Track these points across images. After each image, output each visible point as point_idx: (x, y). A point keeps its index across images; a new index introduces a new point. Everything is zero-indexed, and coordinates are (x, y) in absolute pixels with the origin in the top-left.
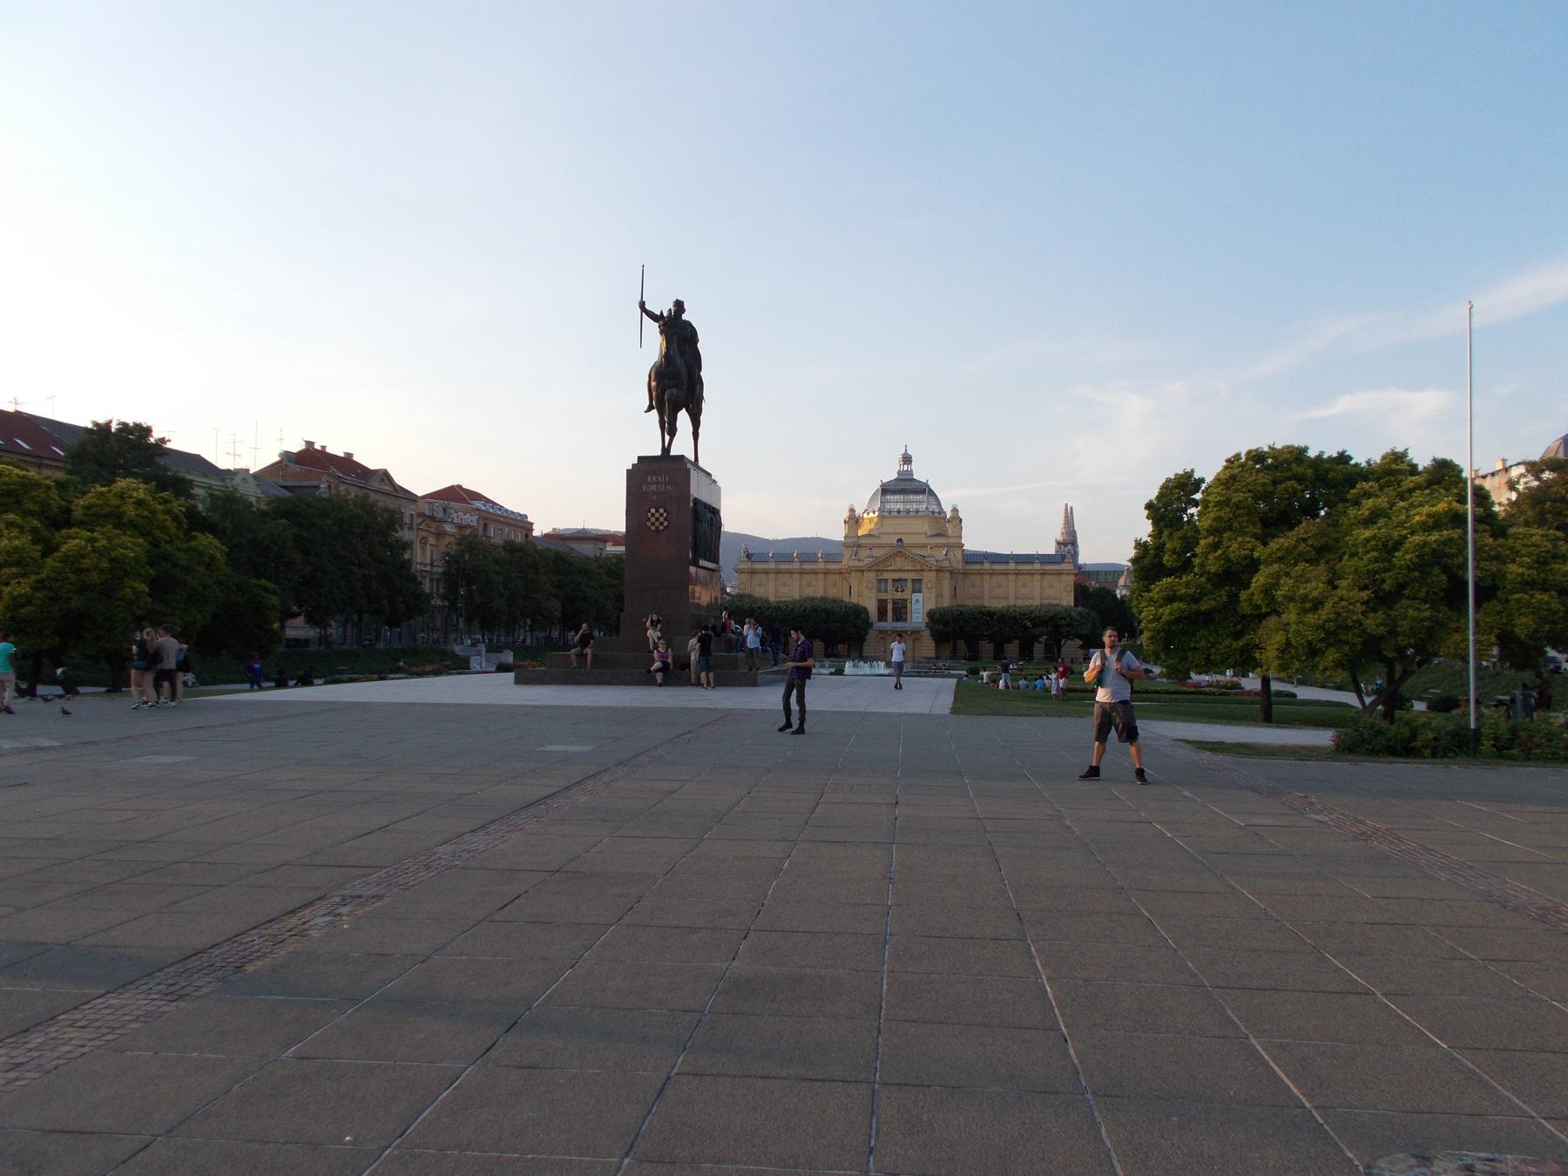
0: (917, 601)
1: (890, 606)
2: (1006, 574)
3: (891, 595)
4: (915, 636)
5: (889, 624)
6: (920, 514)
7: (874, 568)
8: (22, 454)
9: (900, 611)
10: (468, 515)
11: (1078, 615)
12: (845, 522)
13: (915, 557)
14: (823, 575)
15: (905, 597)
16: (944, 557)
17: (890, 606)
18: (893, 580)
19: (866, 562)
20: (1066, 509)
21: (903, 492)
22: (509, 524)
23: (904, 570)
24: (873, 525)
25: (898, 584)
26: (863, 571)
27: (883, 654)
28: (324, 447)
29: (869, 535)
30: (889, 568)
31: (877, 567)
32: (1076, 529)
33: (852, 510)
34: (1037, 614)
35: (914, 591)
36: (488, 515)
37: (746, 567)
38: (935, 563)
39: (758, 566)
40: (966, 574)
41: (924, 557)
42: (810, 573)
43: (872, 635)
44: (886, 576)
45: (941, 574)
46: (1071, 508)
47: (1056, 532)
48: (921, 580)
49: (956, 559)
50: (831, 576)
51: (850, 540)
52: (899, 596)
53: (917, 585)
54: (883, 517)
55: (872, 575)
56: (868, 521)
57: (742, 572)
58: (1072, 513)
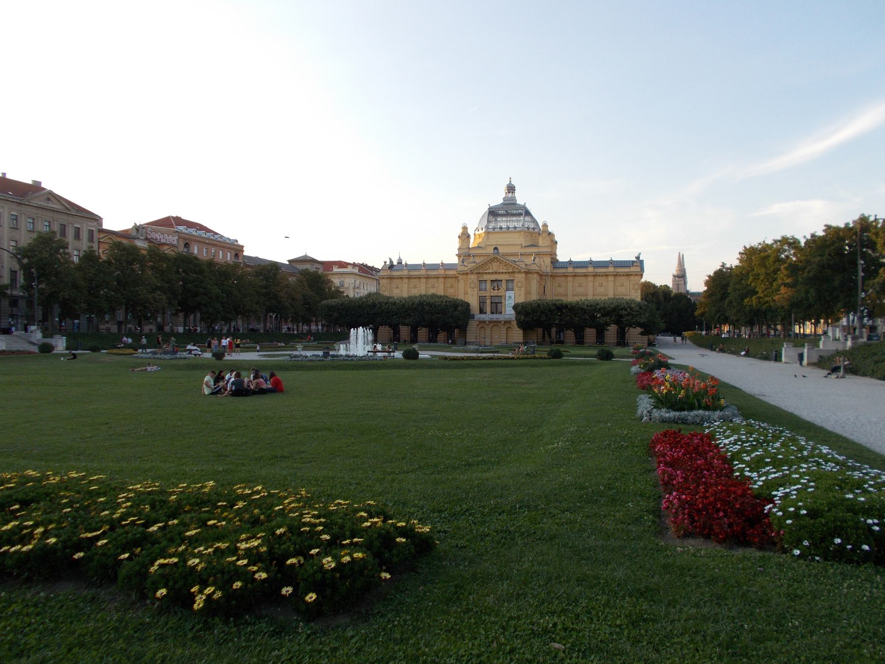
0: (510, 297)
1: (488, 302)
3: (489, 292)
4: (507, 326)
5: (488, 317)
6: (517, 229)
7: (476, 271)
8: (342, 274)
9: (496, 306)
10: (171, 236)
11: (637, 306)
12: (459, 237)
13: (508, 262)
14: (443, 279)
16: (533, 262)
17: (488, 302)
18: (492, 281)
20: (679, 256)
21: (507, 214)
22: (215, 245)
23: (499, 273)
24: (481, 239)
25: (495, 284)
26: (467, 274)
27: (483, 340)
29: (478, 247)
30: (488, 271)
31: (478, 271)
32: (685, 267)
33: (465, 228)
34: (602, 305)
35: (507, 290)
36: (191, 237)
37: (386, 274)
38: (524, 266)
39: (395, 273)
40: (553, 276)
41: (515, 262)
42: (398, 278)
43: (472, 326)
44: (485, 277)
45: (530, 276)
46: (683, 255)
47: (674, 270)
49: (545, 264)
50: (449, 280)
51: (462, 251)
52: (495, 293)
53: (510, 285)
54: (489, 233)
55: (473, 277)
56: (478, 236)
58: (683, 258)
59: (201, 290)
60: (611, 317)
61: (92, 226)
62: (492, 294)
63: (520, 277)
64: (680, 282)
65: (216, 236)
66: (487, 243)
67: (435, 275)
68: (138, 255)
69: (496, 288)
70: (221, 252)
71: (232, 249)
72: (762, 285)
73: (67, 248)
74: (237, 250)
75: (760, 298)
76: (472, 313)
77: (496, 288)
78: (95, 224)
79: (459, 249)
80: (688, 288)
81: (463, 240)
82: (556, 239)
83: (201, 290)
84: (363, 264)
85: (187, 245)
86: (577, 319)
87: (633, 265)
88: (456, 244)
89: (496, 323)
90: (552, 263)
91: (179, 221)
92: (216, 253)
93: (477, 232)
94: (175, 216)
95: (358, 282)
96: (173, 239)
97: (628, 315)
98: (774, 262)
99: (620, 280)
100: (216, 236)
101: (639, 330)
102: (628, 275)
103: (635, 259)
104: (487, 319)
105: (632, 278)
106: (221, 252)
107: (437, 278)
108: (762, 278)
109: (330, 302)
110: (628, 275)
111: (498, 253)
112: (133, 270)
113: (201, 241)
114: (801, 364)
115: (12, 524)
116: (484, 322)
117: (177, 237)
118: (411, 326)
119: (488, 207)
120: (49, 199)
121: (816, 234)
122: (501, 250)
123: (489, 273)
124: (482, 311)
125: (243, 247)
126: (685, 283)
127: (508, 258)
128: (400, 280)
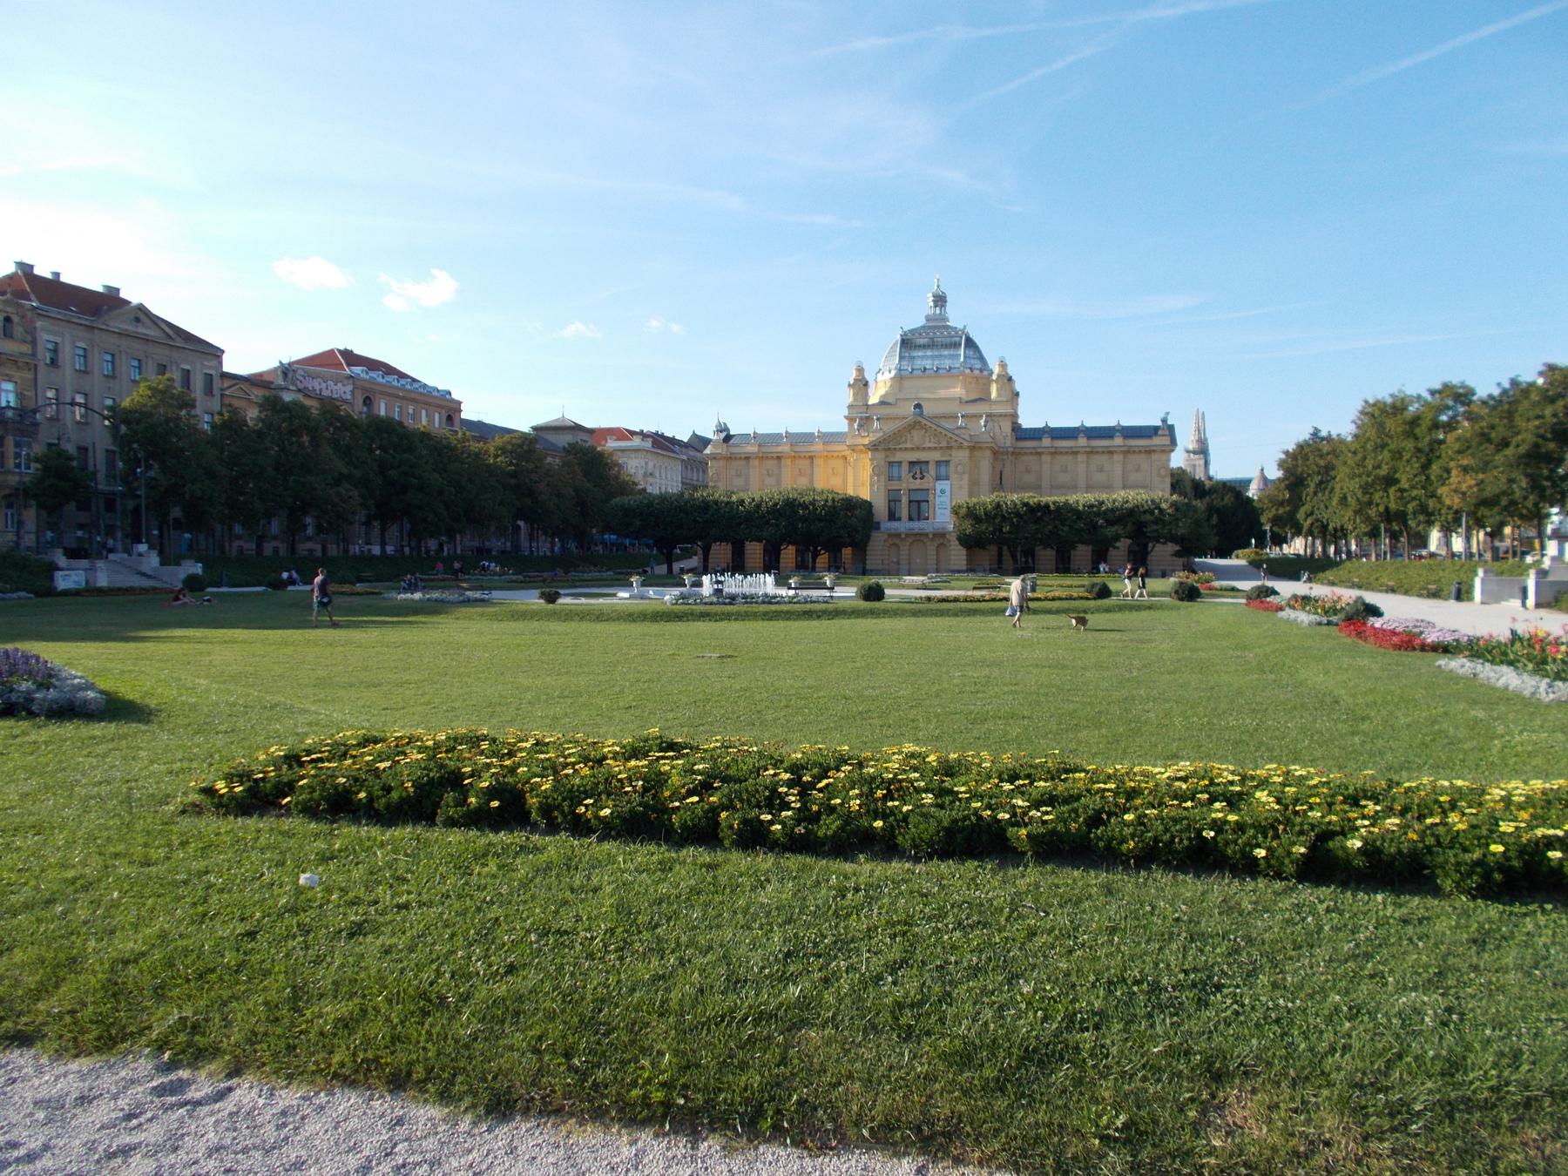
1: (905, 500)
3: (907, 483)
4: (940, 541)
5: (903, 526)
9: (919, 507)
21: (932, 345)
22: (414, 401)
35: (938, 478)
40: (1017, 454)
44: (899, 456)
52: (917, 484)
53: (943, 469)
59: (414, 481)
60: (1125, 526)
61: (210, 368)
62: (912, 487)
63: (961, 456)
64: (1197, 463)
65: (416, 385)
66: (901, 396)
68: (308, 419)
69: (918, 476)
70: (424, 412)
71: (442, 407)
72: (1408, 469)
73: (194, 406)
74: (450, 408)
75: (1402, 491)
76: (876, 519)
77: (918, 476)
80: (1212, 473)
82: (1018, 387)
83: (414, 481)
84: (657, 434)
85: (368, 401)
86: (1066, 529)
87: (1156, 434)
89: (920, 537)
90: (1013, 430)
91: (351, 357)
92: (416, 417)
93: (879, 375)
94: (342, 348)
95: (651, 465)
96: (342, 391)
97: (1156, 522)
98: (1430, 429)
99: (1135, 459)
100: (416, 385)
101: (1171, 547)
102: (1149, 451)
103: (1160, 424)
104: (903, 530)
105: (1155, 457)
106: (424, 412)
107: (1109, 452)
108: (1407, 456)
109: (625, 500)
110: (1149, 451)
111: (921, 414)
112: (301, 445)
113: (391, 395)
114: (1524, 605)
116: (898, 535)
117: (351, 387)
118: (768, 541)
120: (138, 320)
121: (1521, 379)
124: (892, 516)
125: (459, 403)
126: (1207, 463)
127: (943, 423)
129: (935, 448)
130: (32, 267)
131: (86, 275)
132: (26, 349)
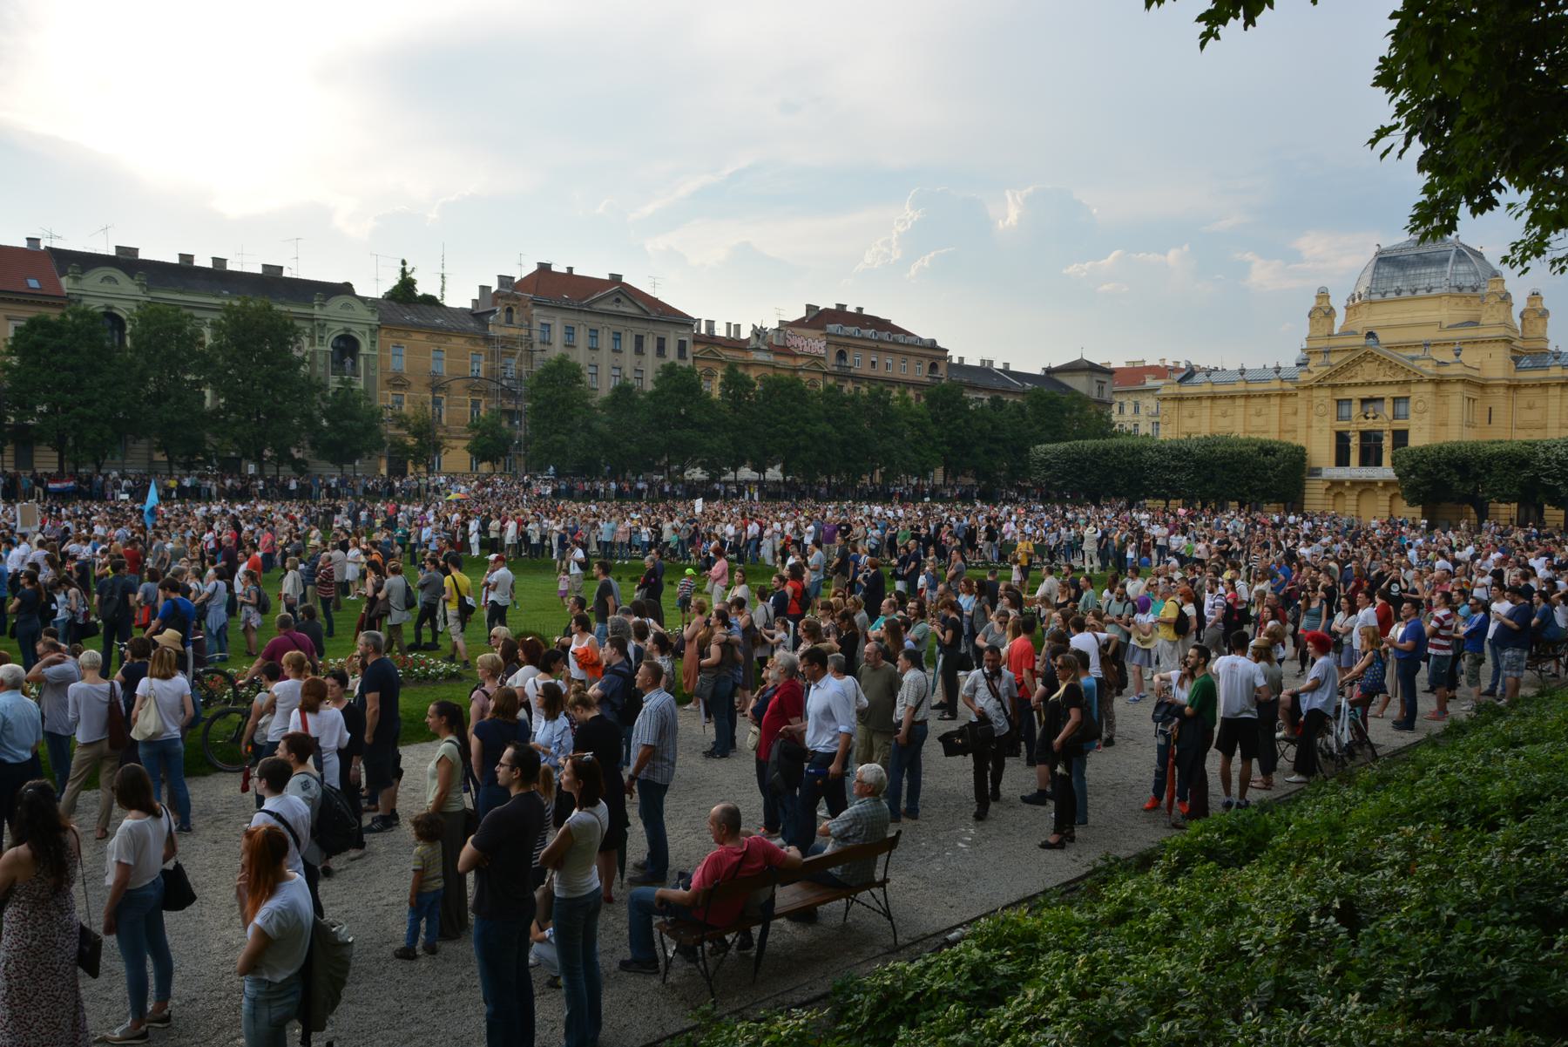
1: (1355, 442)
2: (1544, 386)
3: (1356, 424)
5: (1355, 471)
6: (1434, 292)
7: (1329, 382)
15: (1378, 427)
17: (1355, 442)
19: (1315, 375)
23: (1377, 383)
25: (1370, 407)
26: (1311, 388)
28: (860, 309)
33: (1323, 295)
42: (1534, 386)
44: (1348, 393)
48: (1407, 398)
52: (1369, 425)
53: (1402, 408)
55: (1324, 395)
57: (1165, 399)
61: (683, 335)
67: (1539, 379)
78: (688, 331)
79: (1309, 339)
81: (1318, 322)
85: (841, 355)
88: (1303, 328)
115: (634, 763)
119: (1376, 249)
122: (1384, 337)
123: (1356, 384)
128: (1229, 401)
129: (1391, 383)
130: (549, 266)
131: (594, 268)
132: (524, 332)
